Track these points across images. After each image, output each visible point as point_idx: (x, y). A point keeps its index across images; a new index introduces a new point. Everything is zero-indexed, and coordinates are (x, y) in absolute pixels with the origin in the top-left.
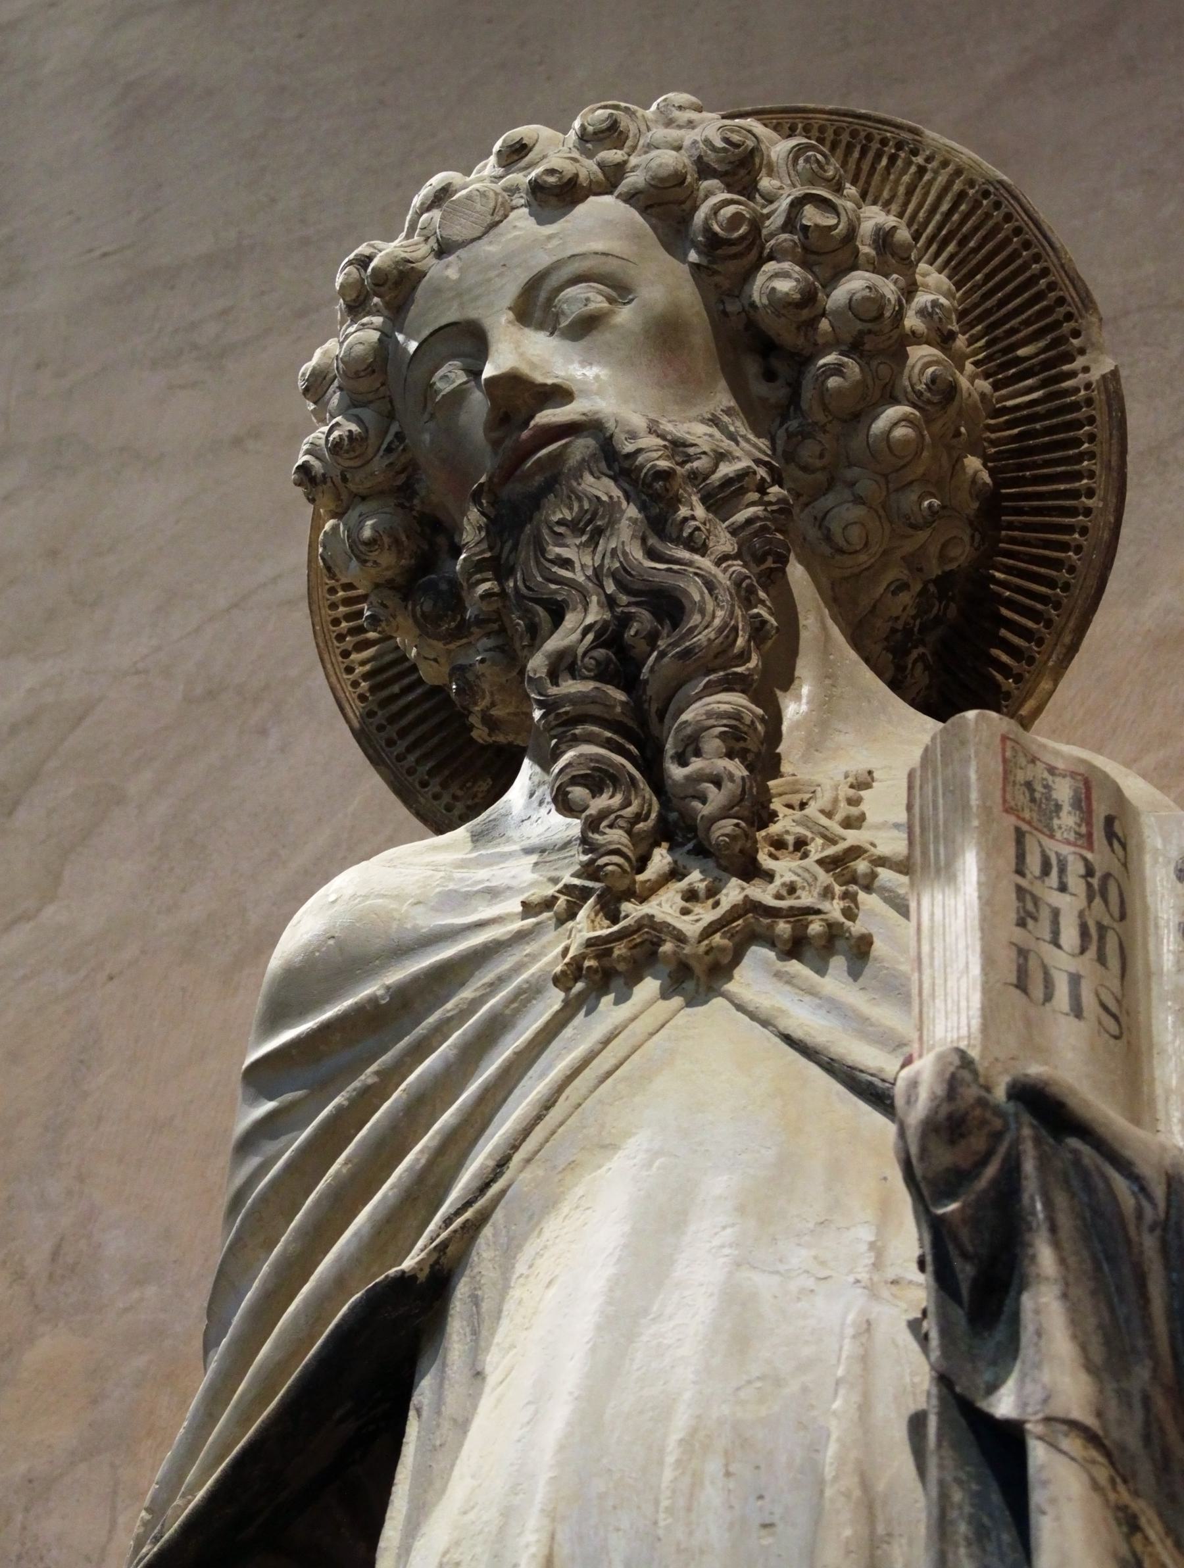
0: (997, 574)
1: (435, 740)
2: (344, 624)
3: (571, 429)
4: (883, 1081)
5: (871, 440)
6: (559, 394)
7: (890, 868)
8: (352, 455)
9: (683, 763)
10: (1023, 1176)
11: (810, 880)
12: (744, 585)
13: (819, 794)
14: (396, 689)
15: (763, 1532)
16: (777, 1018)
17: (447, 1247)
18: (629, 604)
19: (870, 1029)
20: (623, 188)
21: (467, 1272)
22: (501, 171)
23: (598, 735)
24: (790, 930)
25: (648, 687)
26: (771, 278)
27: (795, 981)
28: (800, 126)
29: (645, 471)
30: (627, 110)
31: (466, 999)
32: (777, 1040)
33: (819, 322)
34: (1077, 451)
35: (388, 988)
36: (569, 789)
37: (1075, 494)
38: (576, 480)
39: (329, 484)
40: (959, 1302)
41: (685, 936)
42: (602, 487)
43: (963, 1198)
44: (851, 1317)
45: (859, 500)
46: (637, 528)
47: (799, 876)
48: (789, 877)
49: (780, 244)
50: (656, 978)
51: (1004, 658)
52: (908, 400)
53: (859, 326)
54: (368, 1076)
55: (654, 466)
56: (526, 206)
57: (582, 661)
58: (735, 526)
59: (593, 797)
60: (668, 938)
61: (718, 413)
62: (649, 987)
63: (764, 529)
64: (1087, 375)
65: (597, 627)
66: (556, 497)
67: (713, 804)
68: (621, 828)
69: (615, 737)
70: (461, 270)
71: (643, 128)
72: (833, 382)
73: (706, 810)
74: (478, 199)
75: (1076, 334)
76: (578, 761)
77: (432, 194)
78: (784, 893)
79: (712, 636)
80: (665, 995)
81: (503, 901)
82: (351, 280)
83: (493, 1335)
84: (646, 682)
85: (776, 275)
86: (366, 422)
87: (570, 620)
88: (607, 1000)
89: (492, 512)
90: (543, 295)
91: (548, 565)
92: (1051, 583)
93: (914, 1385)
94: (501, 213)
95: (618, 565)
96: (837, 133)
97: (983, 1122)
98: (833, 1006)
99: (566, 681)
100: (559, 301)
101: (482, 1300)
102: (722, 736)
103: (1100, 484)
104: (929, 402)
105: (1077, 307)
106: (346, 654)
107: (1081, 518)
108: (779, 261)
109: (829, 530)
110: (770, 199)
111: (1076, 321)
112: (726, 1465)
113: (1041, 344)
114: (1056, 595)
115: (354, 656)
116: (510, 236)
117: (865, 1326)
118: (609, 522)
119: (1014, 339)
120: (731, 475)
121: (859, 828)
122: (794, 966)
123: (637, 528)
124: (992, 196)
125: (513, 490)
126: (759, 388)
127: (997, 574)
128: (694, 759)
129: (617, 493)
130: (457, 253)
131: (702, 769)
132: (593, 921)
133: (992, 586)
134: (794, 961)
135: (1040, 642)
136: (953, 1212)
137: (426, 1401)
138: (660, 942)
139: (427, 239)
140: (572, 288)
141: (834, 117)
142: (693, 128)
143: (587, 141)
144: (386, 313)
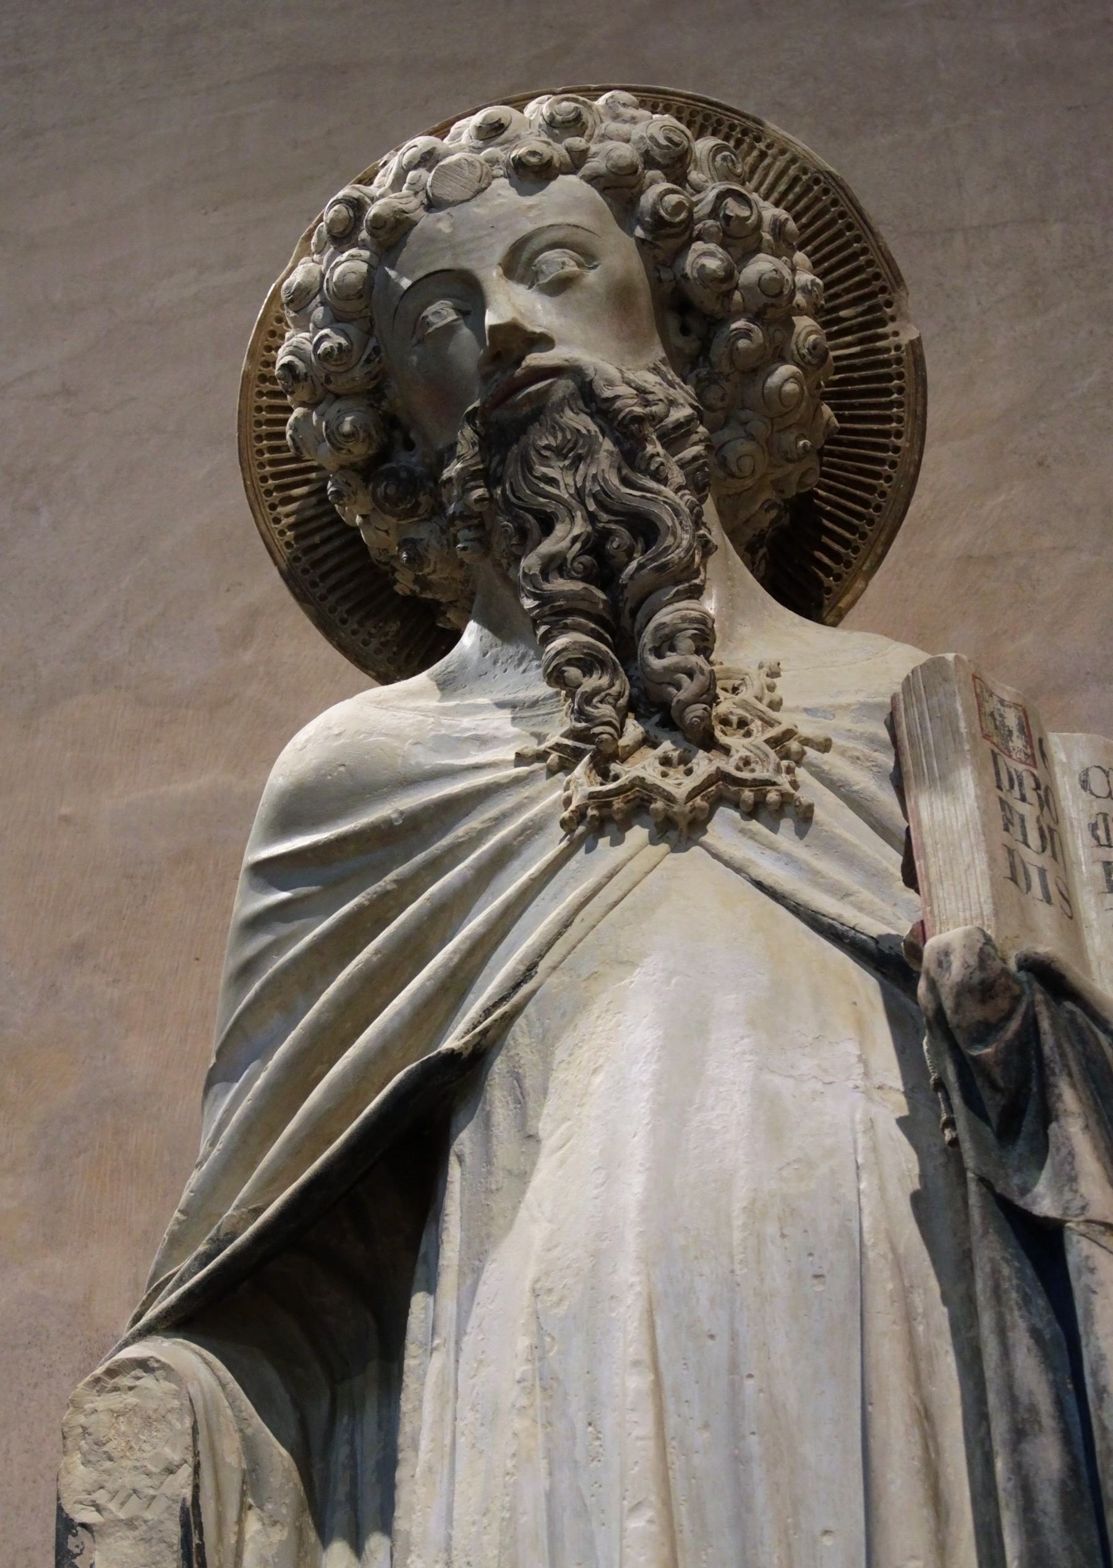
0: (820, 492)
1: (352, 585)
2: (270, 482)
3: (556, 371)
4: (843, 924)
5: (766, 391)
6: (544, 341)
7: (812, 747)
8: (339, 362)
9: (660, 656)
10: (1042, 1031)
11: (762, 756)
12: (695, 511)
13: (748, 681)
14: (317, 539)
15: (815, 1281)
16: (749, 867)
17: (488, 1032)
18: (609, 522)
19: (821, 880)
20: (587, 168)
21: (504, 1052)
22: (480, 143)
23: (585, 626)
24: (752, 797)
25: (625, 590)
26: (699, 256)
27: (757, 837)
28: (661, 105)
29: (623, 414)
30: (584, 103)
31: (475, 828)
32: (750, 884)
33: (733, 294)
34: (888, 399)
35: (402, 813)
36: (564, 668)
37: (886, 434)
38: (558, 413)
39: (309, 381)
40: (985, 1119)
41: (674, 797)
42: (580, 421)
43: (994, 1046)
44: (858, 1116)
45: (751, 437)
46: (613, 459)
47: (751, 752)
48: (744, 753)
49: (708, 228)
50: (643, 826)
51: (826, 560)
52: (794, 361)
53: (764, 300)
54: (387, 881)
55: (632, 411)
56: (506, 177)
57: (572, 564)
58: (683, 461)
59: (584, 676)
60: (659, 798)
61: (658, 363)
62: (638, 834)
63: (705, 464)
64: (896, 339)
65: (583, 538)
66: (540, 425)
67: (688, 692)
68: (610, 703)
69: (597, 628)
70: (452, 225)
71: (598, 121)
72: (742, 343)
73: (682, 695)
74: (466, 167)
75: (889, 304)
76: (574, 647)
77: (419, 155)
78: (741, 765)
79: (682, 555)
80: (653, 841)
81: (490, 748)
82: (341, 217)
83: (542, 1106)
84: (625, 586)
85: (704, 254)
86: (352, 338)
87: (560, 529)
88: (604, 842)
89: (480, 429)
90: (525, 256)
91: (536, 481)
92: (865, 504)
93: (909, 1170)
94: (486, 181)
95: (599, 488)
96: (692, 114)
97: (1008, 988)
98: (790, 860)
99: (556, 579)
100: (539, 262)
101: (525, 1077)
102: (693, 637)
103: (908, 428)
104: (809, 363)
105: (891, 283)
106: (273, 507)
107: (890, 453)
108: (706, 242)
109: (725, 458)
110: (698, 190)
111: (890, 294)
112: (781, 1228)
113: (860, 309)
114: (870, 514)
115: (280, 509)
116: (496, 203)
117: (870, 1124)
118: (589, 450)
119: (838, 302)
120: (682, 420)
121: (778, 710)
122: (755, 825)
123: (613, 459)
124: (822, 184)
125: (501, 415)
126: (679, 341)
127: (820, 492)
128: (669, 653)
129: (594, 428)
130: (448, 210)
131: (678, 663)
132: (589, 777)
133: (816, 501)
134: (754, 821)
135: (856, 550)
136: (987, 1055)
137: (467, 1151)
138: (651, 800)
139: (416, 193)
140: (550, 252)
141: (690, 101)
142: (635, 123)
143: (554, 127)
144: (374, 248)
